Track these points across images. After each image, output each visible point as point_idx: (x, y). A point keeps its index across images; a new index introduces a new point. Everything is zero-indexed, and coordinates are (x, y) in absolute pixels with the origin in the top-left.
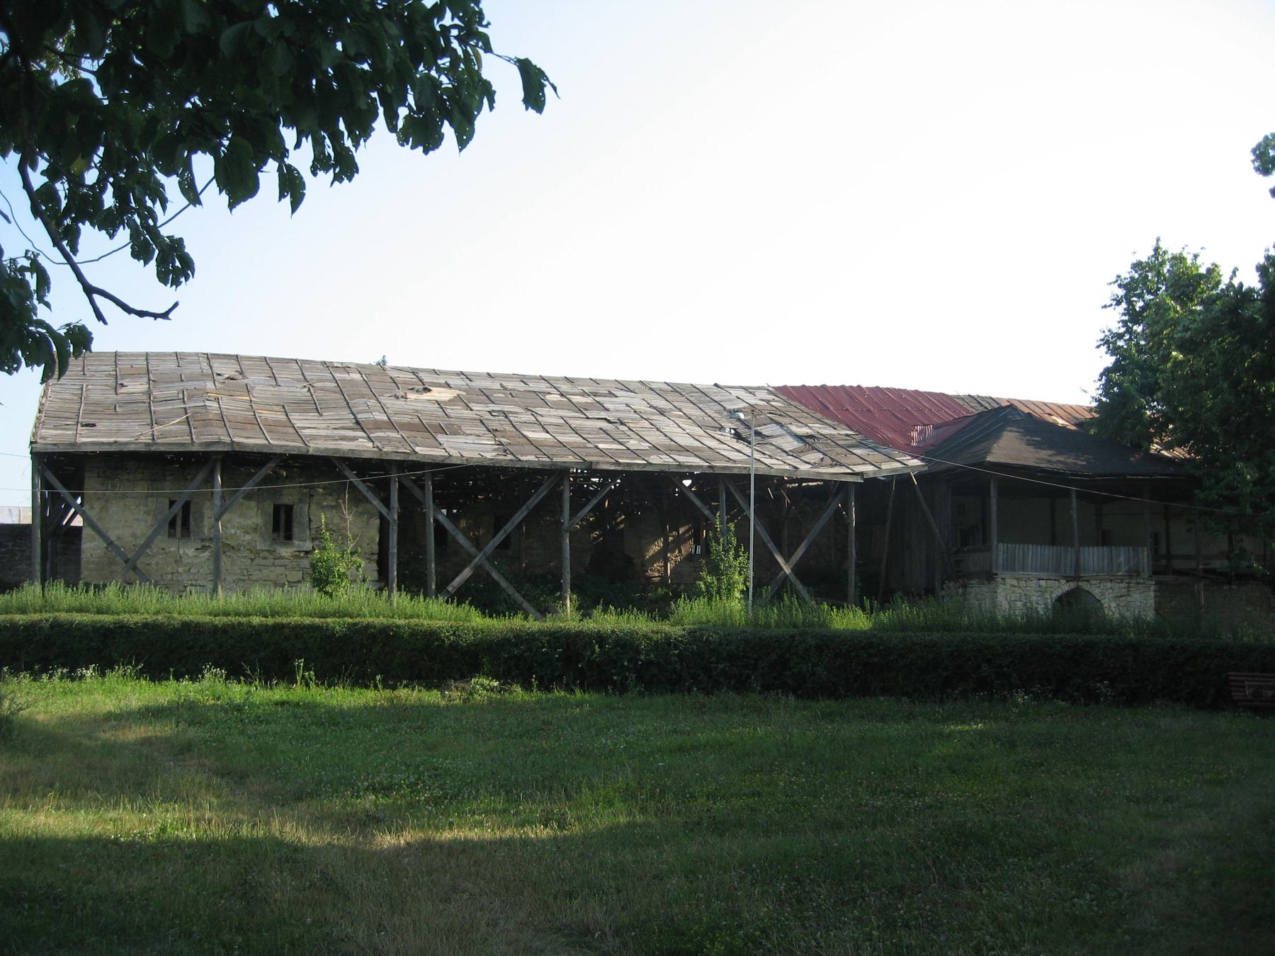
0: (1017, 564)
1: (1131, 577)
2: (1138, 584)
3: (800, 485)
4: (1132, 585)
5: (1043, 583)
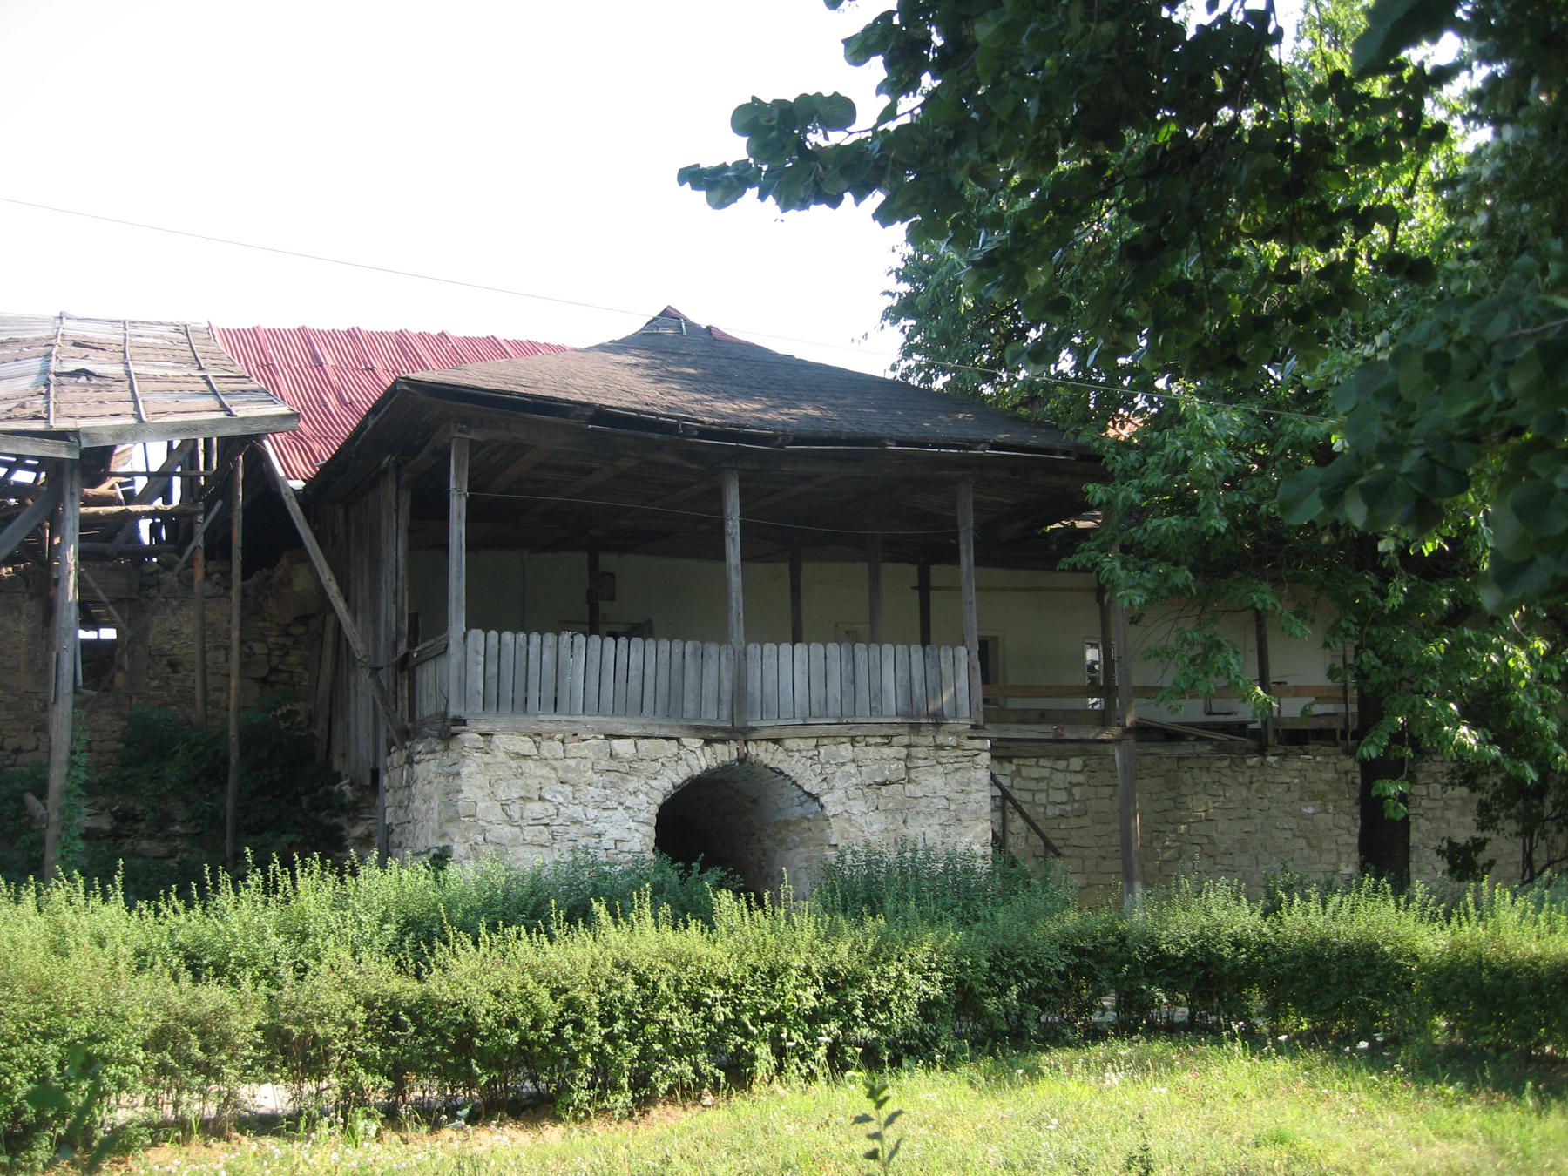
1: (915, 728)
2: (941, 747)
5: (623, 747)
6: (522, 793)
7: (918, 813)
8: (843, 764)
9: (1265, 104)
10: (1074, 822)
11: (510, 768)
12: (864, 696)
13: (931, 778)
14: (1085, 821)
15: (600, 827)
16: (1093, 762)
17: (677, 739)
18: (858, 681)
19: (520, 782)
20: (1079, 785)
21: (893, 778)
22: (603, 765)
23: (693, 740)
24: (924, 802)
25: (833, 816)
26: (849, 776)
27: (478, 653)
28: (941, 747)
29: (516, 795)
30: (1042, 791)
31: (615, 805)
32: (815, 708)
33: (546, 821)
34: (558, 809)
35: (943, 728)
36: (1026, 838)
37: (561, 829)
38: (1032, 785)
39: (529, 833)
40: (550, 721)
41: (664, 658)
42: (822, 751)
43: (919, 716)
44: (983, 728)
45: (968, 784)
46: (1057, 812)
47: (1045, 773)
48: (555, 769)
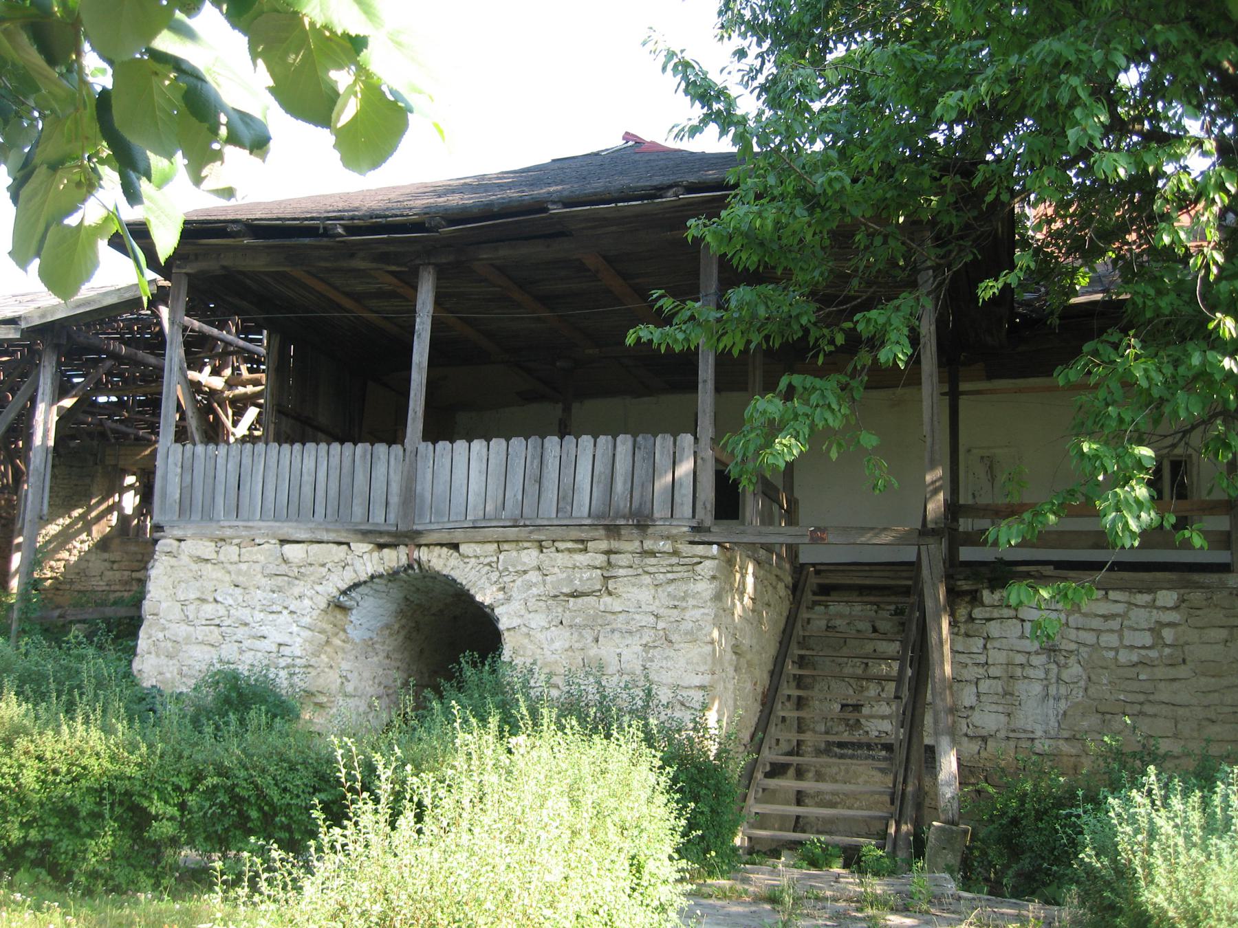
0: (220, 501)
1: (613, 531)
2: (652, 554)
3: (246, 337)
4: (622, 560)
6: (198, 595)
7: (613, 631)
8: (525, 572)
10: (1160, 672)
11: (191, 570)
12: (550, 495)
13: (635, 590)
14: (1182, 672)
15: (264, 630)
16: (1197, 596)
17: (348, 544)
18: (544, 480)
19: (198, 584)
20: (1170, 625)
21: (585, 589)
22: (272, 569)
23: (361, 545)
24: (622, 617)
25: (508, 629)
26: (530, 585)
27: (176, 465)
28: (652, 554)
29: (192, 596)
30: (1112, 631)
31: (279, 609)
33: (217, 621)
34: (229, 611)
35: (650, 530)
36: (1086, 690)
37: (229, 630)
38: (1096, 623)
39: (200, 632)
40: (230, 527)
41: (335, 461)
42: (501, 557)
44: (708, 530)
45: (684, 599)
46: (1135, 658)
47: (1119, 609)
48: (229, 572)
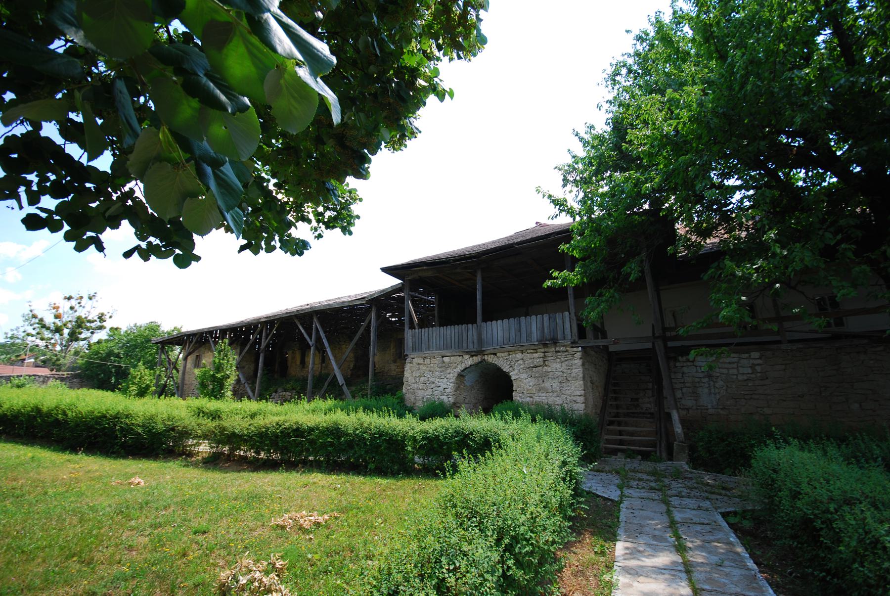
1: (545, 345)
2: (557, 352)
4: (550, 354)
5: (446, 359)
9: (60, 92)
12: (524, 335)
22: (440, 365)
32: (505, 342)
38: (726, 366)
41: (456, 331)
43: (546, 340)
44: (577, 343)
